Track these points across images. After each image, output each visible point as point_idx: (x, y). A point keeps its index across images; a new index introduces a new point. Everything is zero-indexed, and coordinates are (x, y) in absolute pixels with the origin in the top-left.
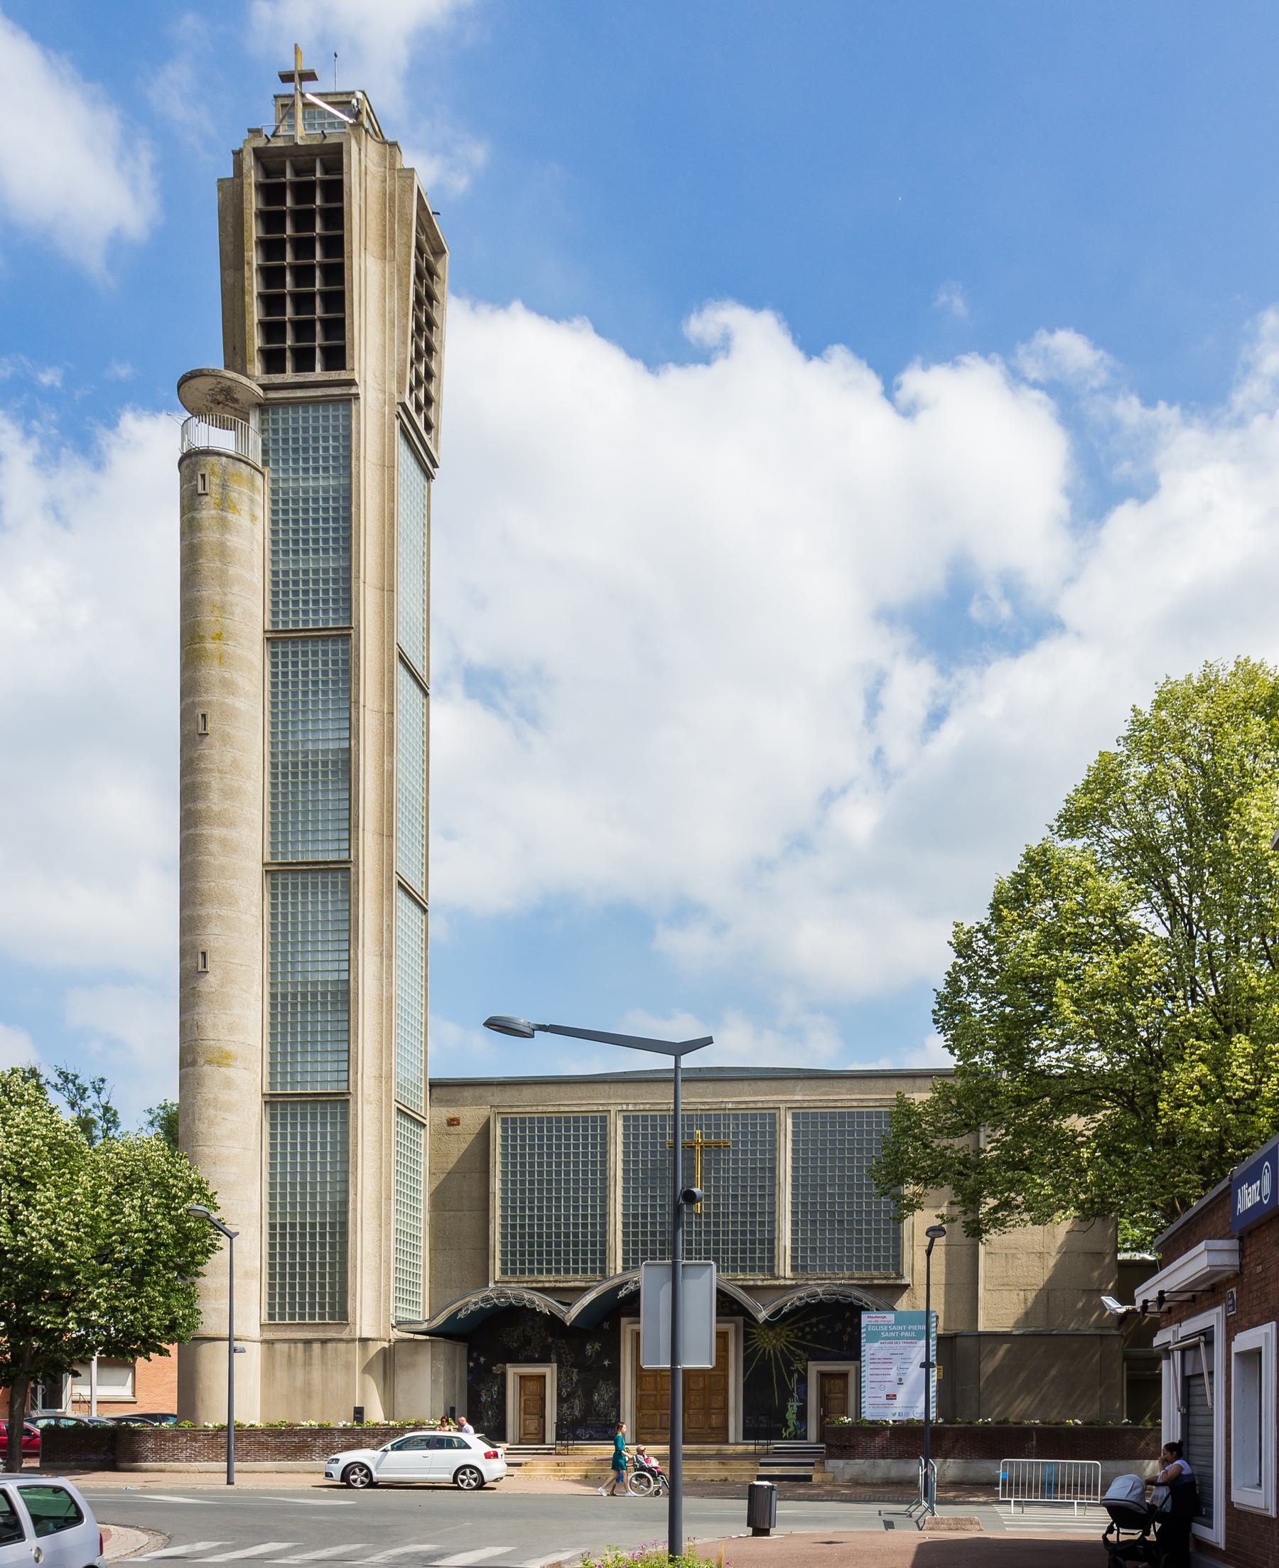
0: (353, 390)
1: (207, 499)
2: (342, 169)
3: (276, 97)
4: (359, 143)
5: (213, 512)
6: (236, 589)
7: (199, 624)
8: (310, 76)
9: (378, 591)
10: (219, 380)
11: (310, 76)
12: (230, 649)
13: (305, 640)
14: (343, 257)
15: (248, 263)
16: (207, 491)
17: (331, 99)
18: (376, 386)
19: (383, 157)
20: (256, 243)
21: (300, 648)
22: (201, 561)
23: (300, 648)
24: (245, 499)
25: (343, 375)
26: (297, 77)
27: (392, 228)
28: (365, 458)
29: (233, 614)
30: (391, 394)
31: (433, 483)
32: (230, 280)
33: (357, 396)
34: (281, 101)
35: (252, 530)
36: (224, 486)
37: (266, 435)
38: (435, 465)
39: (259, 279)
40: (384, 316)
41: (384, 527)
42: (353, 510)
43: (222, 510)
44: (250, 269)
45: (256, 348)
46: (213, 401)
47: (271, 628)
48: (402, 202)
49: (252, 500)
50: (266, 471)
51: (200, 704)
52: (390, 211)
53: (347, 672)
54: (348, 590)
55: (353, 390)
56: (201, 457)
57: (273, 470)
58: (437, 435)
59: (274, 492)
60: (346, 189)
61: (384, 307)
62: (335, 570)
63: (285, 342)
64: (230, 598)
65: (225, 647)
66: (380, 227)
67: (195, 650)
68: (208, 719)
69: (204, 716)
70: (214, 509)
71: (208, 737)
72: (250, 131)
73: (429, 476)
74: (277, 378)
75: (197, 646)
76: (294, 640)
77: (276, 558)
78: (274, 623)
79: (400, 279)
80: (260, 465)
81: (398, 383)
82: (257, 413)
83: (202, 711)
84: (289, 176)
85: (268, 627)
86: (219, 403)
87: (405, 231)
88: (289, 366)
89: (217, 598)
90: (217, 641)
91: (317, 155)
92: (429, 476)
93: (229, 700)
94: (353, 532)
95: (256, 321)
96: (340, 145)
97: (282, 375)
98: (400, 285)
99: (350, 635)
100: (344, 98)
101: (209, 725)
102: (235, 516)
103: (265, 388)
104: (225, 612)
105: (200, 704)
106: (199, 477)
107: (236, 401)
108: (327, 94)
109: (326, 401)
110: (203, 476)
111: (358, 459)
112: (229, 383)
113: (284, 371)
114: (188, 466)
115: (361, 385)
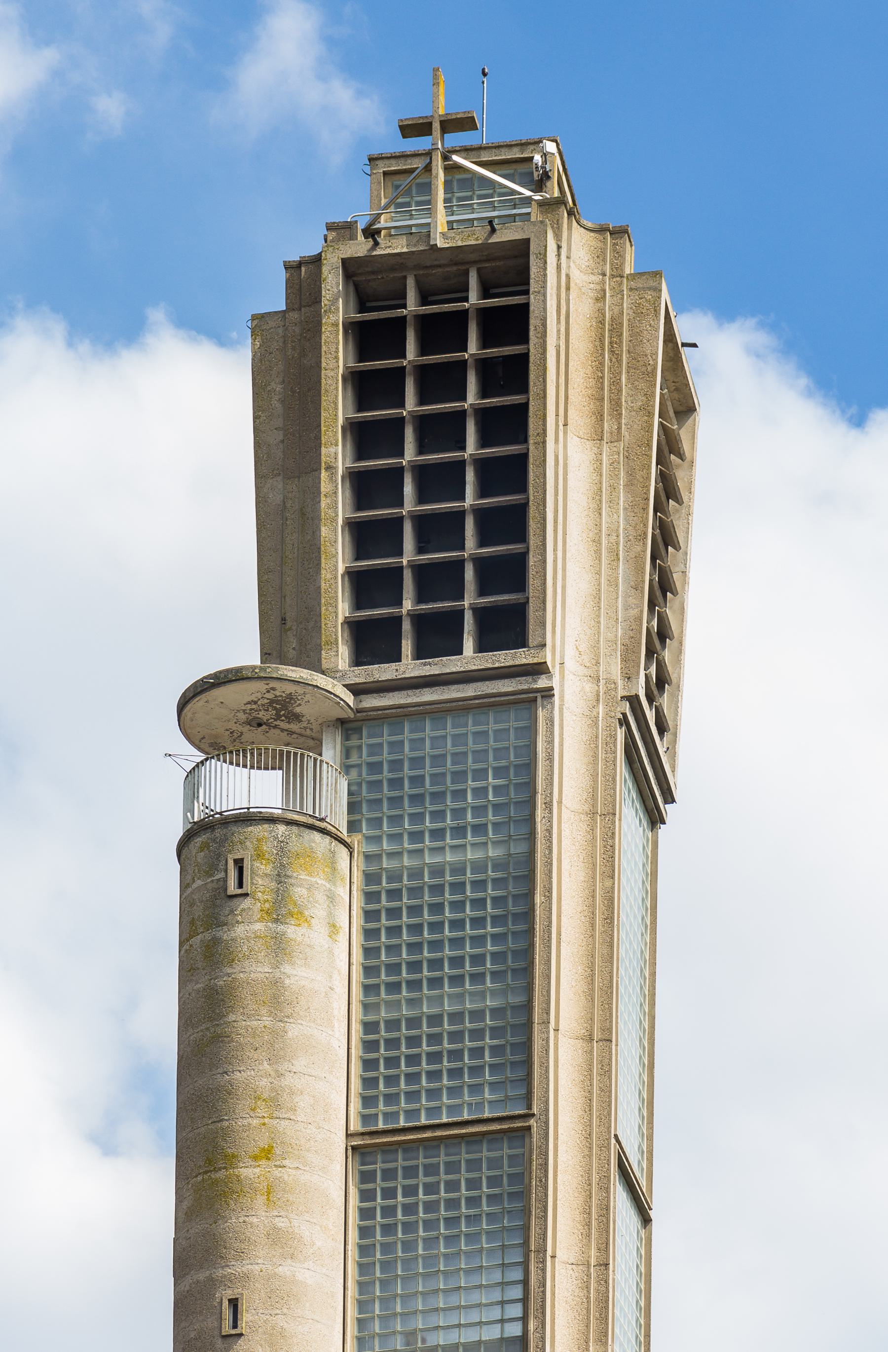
0: (542, 683)
1: (247, 903)
2: (527, 283)
3: (371, 159)
4: (558, 237)
5: (258, 926)
6: (300, 1064)
7: (225, 1133)
8: (467, 123)
9: (580, 1043)
10: (273, 684)
11: (467, 123)
12: (288, 1175)
13: (432, 1145)
14: (526, 441)
15: (329, 468)
16: (247, 887)
17: (486, 157)
18: (582, 671)
19: (600, 256)
20: (344, 428)
21: (401, 1163)
22: (232, 1017)
23: (401, 1163)
24: (320, 897)
25: (522, 657)
26: (436, 126)
27: (616, 383)
28: (560, 802)
29: (294, 1110)
30: (608, 681)
31: (663, 830)
32: (275, 498)
33: (548, 693)
34: (382, 167)
35: (331, 952)
36: (281, 877)
37: (354, 773)
38: (669, 798)
39: (348, 493)
40: (597, 541)
41: (593, 925)
42: (538, 899)
43: (276, 921)
44: (332, 478)
45: (341, 619)
46: (249, 723)
47: (360, 1129)
48: (635, 334)
49: (331, 898)
50: (356, 840)
51: (228, 1281)
52: (612, 352)
53: (522, 1195)
54: (527, 1046)
55: (542, 683)
56: (234, 828)
57: (369, 839)
58: (674, 742)
59: (370, 878)
60: (533, 322)
61: (598, 525)
62: (496, 1012)
63: (400, 604)
64: (288, 1081)
65: (277, 1172)
66: (592, 382)
67: (216, 1182)
68: (243, 1306)
69: (234, 1304)
70: (262, 919)
71: (241, 1341)
72: (330, 227)
73: (655, 819)
74: (384, 672)
75: (221, 1174)
76: (408, 1147)
77: (372, 999)
78: (366, 1119)
79: (630, 474)
80: (345, 832)
81: (624, 660)
82: (339, 739)
83: (229, 1294)
84: (412, 305)
85: (356, 1125)
86: (260, 725)
87: (642, 385)
88: (407, 646)
89: (264, 1082)
90: (263, 1162)
91: (475, 262)
92: (655, 819)
93: (285, 1269)
94: (537, 940)
95: (341, 569)
96: (525, 243)
97: (394, 665)
98: (629, 484)
99: (529, 1128)
100: (516, 154)
101: (246, 1318)
102: (301, 930)
103: (357, 690)
104: (278, 1107)
105: (228, 1281)
106: (231, 864)
107: (297, 717)
108: (480, 148)
109: (479, 706)
110: (239, 864)
111: (549, 806)
112: (290, 688)
113: (396, 657)
114: (205, 846)
115: (555, 671)
